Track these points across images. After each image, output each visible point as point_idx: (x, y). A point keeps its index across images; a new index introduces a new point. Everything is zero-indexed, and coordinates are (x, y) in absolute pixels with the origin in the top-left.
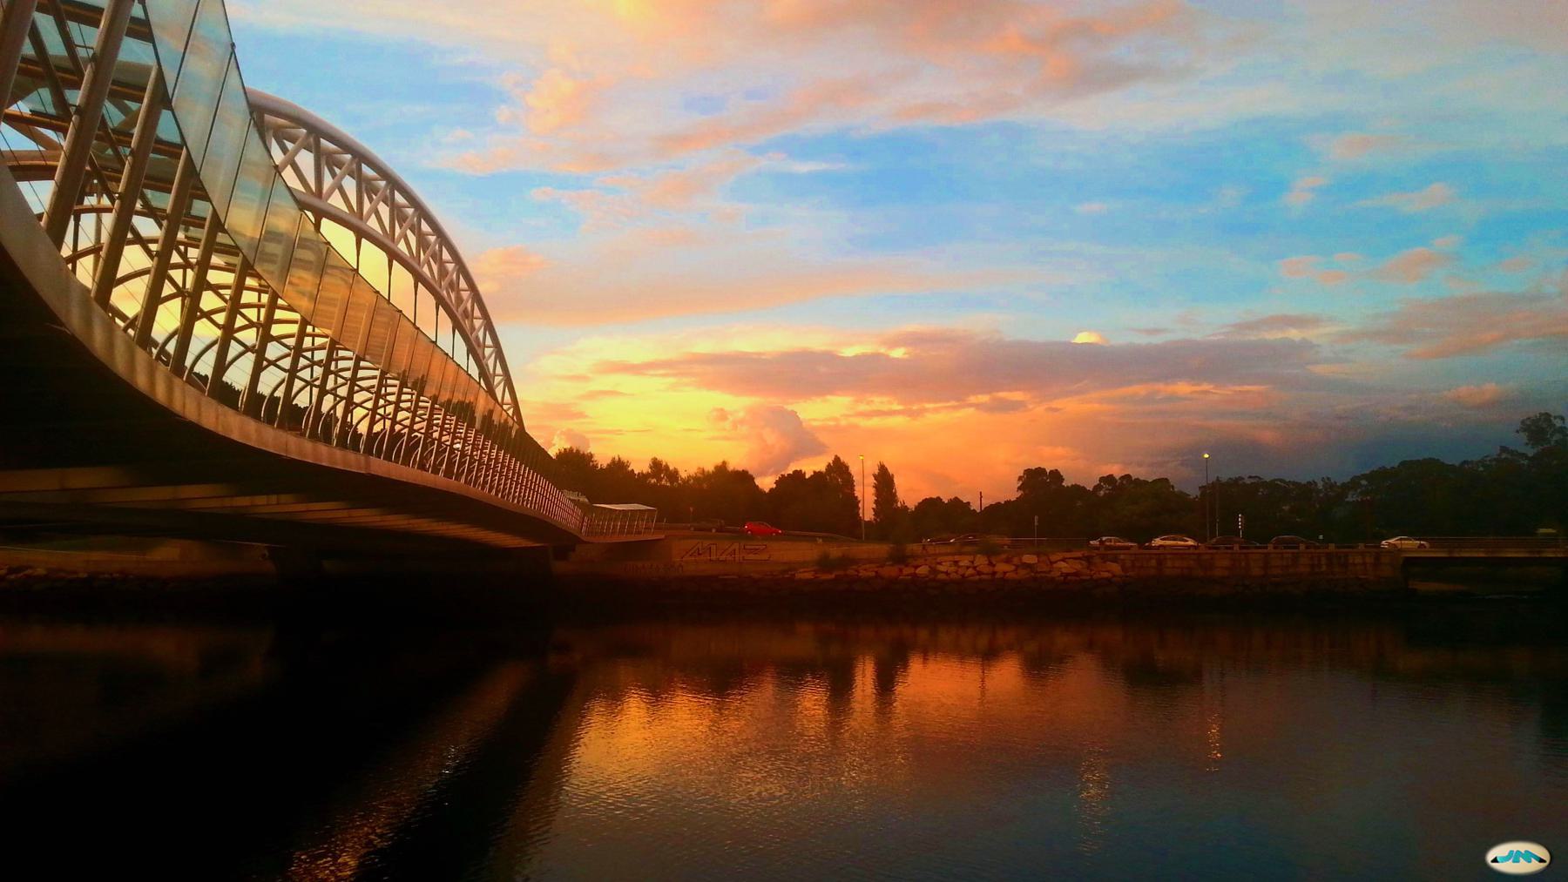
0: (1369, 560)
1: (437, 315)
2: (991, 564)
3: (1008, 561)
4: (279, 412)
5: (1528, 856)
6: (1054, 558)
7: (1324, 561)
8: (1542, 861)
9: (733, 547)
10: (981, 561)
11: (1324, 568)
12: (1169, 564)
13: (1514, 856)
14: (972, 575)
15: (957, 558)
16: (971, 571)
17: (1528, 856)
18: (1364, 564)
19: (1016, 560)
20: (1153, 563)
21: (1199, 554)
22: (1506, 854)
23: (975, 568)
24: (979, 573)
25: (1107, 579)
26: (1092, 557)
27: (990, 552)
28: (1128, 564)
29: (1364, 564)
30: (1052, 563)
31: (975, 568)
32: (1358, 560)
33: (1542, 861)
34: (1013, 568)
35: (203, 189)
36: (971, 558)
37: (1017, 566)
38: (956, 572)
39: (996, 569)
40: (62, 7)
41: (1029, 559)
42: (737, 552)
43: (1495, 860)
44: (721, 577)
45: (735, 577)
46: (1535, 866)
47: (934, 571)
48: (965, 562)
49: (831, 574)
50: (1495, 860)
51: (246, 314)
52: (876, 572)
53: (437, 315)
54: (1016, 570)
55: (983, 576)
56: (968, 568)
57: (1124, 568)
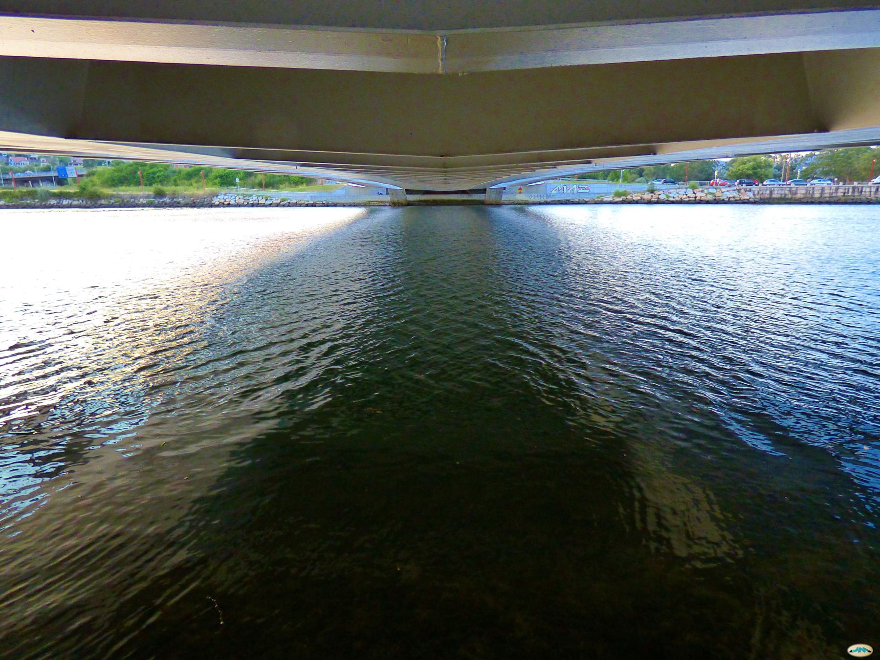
5: (864, 650)
6: (723, 190)
7: (851, 190)
8: (869, 651)
11: (850, 194)
12: (776, 192)
13: (859, 650)
15: (678, 190)
16: (685, 196)
17: (864, 650)
19: (706, 191)
20: (768, 192)
21: (791, 188)
22: (855, 649)
24: (689, 197)
26: (741, 189)
28: (756, 193)
30: (722, 192)
33: (869, 651)
34: (705, 195)
39: (697, 195)
40: (422, 377)
43: (851, 651)
46: (867, 654)
50: (851, 651)
55: (691, 199)
57: (754, 195)
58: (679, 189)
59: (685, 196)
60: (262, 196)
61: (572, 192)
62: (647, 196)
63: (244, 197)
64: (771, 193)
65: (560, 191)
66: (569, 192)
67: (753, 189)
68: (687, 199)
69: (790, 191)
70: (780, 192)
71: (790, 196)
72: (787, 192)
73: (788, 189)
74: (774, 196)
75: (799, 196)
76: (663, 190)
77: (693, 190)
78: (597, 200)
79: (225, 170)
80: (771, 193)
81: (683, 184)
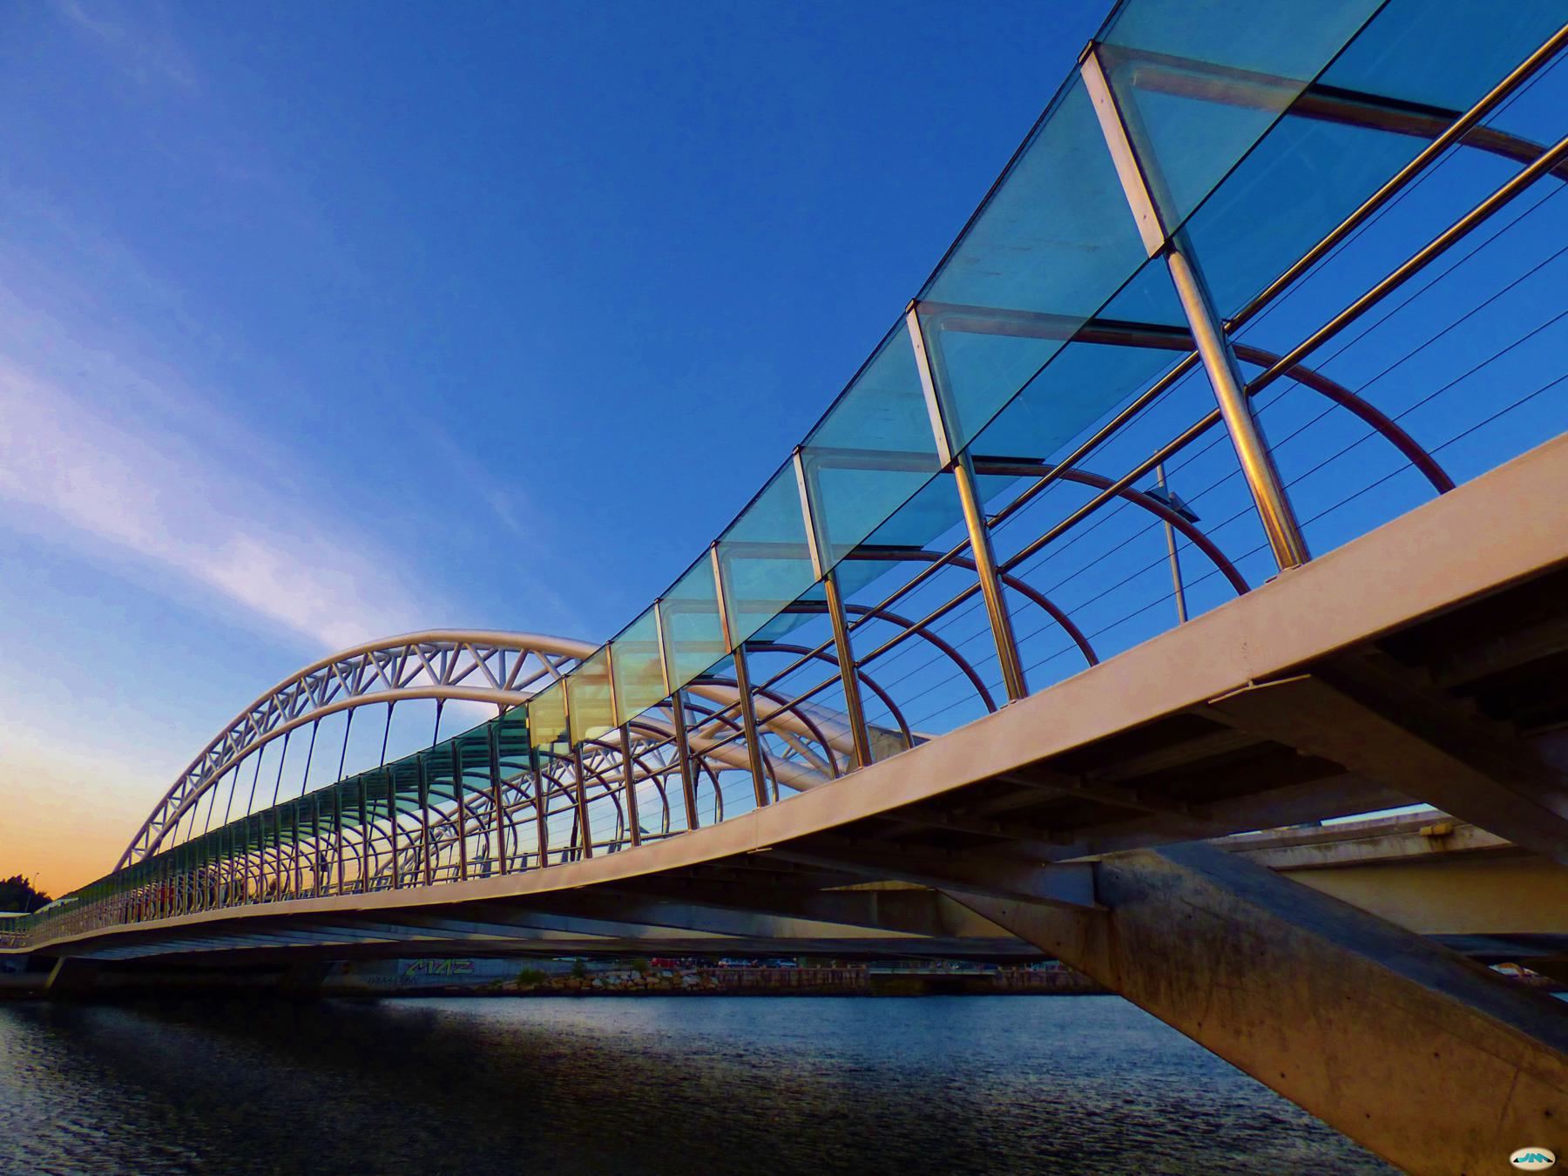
0: (854, 975)
1: (315, 732)
2: (642, 978)
3: (654, 975)
4: (823, 889)
5: (1540, 1158)
7: (830, 976)
8: (1549, 1161)
9: (446, 964)
10: (636, 976)
13: (1530, 1158)
14: (631, 986)
15: (619, 973)
17: (1540, 1158)
18: (851, 978)
20: (736, 977)
22: (1523, 1156)
23: (632, 981)
24: (636, 985)
25: (713, 989)
27: (641, 969)
29: (851, 978)
31: (632, 981)
32: (848, 975)
33: (1549, 1161)
35: (1543, 149)
36: (628, 973)
37: (661, 980)
38: (621, 984)
41: (667, 974)
42: (449, 967)
43: (1516, 1161)
44: (447, 988)
45: (457, 988)
46: (1544, 1165)
47: (606, 984)
48: (625, 976)
49: (531, 984)
50: (1516, 1161)
51: (1176, 534)
52: (564, 984)
53: (315, 732)
54: (660, 982)
56: (628, 981)
58: (619, 970)
59: (630, 983)
60: (341, 893)
61: (442, 972)
62: (574, 982)
63: (362, 881)
64: (740, 979)
65: (422, 971)
66: (437, 972)
67: (718, 973)
68: (635, 988)
69: (762, 976)
70: (750, 978)
71: (762, 984)
72: (759, 978)
73: (759, 973)
74: (744, 983)
75: (773, 984)
76: (598, 971)
77: (641, 973)
78: (491, 988)
79: (660, 1042)
80: (740, 979)
81: (626, 963)
